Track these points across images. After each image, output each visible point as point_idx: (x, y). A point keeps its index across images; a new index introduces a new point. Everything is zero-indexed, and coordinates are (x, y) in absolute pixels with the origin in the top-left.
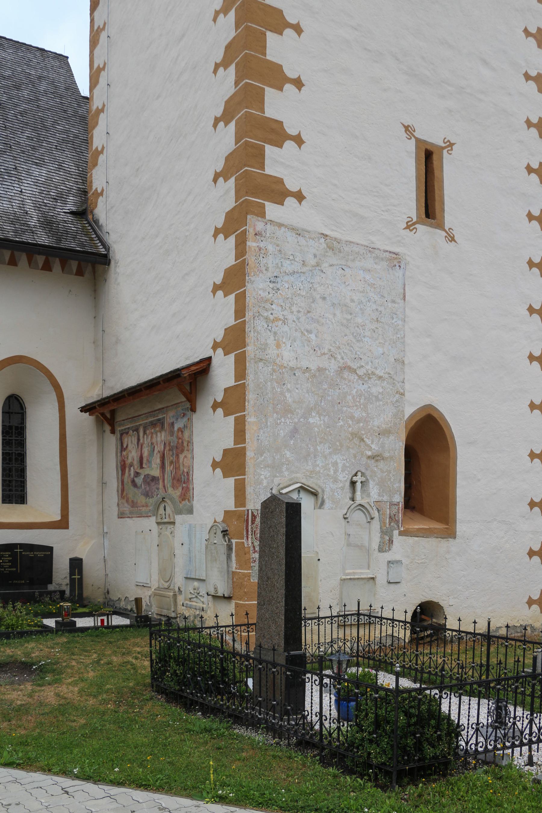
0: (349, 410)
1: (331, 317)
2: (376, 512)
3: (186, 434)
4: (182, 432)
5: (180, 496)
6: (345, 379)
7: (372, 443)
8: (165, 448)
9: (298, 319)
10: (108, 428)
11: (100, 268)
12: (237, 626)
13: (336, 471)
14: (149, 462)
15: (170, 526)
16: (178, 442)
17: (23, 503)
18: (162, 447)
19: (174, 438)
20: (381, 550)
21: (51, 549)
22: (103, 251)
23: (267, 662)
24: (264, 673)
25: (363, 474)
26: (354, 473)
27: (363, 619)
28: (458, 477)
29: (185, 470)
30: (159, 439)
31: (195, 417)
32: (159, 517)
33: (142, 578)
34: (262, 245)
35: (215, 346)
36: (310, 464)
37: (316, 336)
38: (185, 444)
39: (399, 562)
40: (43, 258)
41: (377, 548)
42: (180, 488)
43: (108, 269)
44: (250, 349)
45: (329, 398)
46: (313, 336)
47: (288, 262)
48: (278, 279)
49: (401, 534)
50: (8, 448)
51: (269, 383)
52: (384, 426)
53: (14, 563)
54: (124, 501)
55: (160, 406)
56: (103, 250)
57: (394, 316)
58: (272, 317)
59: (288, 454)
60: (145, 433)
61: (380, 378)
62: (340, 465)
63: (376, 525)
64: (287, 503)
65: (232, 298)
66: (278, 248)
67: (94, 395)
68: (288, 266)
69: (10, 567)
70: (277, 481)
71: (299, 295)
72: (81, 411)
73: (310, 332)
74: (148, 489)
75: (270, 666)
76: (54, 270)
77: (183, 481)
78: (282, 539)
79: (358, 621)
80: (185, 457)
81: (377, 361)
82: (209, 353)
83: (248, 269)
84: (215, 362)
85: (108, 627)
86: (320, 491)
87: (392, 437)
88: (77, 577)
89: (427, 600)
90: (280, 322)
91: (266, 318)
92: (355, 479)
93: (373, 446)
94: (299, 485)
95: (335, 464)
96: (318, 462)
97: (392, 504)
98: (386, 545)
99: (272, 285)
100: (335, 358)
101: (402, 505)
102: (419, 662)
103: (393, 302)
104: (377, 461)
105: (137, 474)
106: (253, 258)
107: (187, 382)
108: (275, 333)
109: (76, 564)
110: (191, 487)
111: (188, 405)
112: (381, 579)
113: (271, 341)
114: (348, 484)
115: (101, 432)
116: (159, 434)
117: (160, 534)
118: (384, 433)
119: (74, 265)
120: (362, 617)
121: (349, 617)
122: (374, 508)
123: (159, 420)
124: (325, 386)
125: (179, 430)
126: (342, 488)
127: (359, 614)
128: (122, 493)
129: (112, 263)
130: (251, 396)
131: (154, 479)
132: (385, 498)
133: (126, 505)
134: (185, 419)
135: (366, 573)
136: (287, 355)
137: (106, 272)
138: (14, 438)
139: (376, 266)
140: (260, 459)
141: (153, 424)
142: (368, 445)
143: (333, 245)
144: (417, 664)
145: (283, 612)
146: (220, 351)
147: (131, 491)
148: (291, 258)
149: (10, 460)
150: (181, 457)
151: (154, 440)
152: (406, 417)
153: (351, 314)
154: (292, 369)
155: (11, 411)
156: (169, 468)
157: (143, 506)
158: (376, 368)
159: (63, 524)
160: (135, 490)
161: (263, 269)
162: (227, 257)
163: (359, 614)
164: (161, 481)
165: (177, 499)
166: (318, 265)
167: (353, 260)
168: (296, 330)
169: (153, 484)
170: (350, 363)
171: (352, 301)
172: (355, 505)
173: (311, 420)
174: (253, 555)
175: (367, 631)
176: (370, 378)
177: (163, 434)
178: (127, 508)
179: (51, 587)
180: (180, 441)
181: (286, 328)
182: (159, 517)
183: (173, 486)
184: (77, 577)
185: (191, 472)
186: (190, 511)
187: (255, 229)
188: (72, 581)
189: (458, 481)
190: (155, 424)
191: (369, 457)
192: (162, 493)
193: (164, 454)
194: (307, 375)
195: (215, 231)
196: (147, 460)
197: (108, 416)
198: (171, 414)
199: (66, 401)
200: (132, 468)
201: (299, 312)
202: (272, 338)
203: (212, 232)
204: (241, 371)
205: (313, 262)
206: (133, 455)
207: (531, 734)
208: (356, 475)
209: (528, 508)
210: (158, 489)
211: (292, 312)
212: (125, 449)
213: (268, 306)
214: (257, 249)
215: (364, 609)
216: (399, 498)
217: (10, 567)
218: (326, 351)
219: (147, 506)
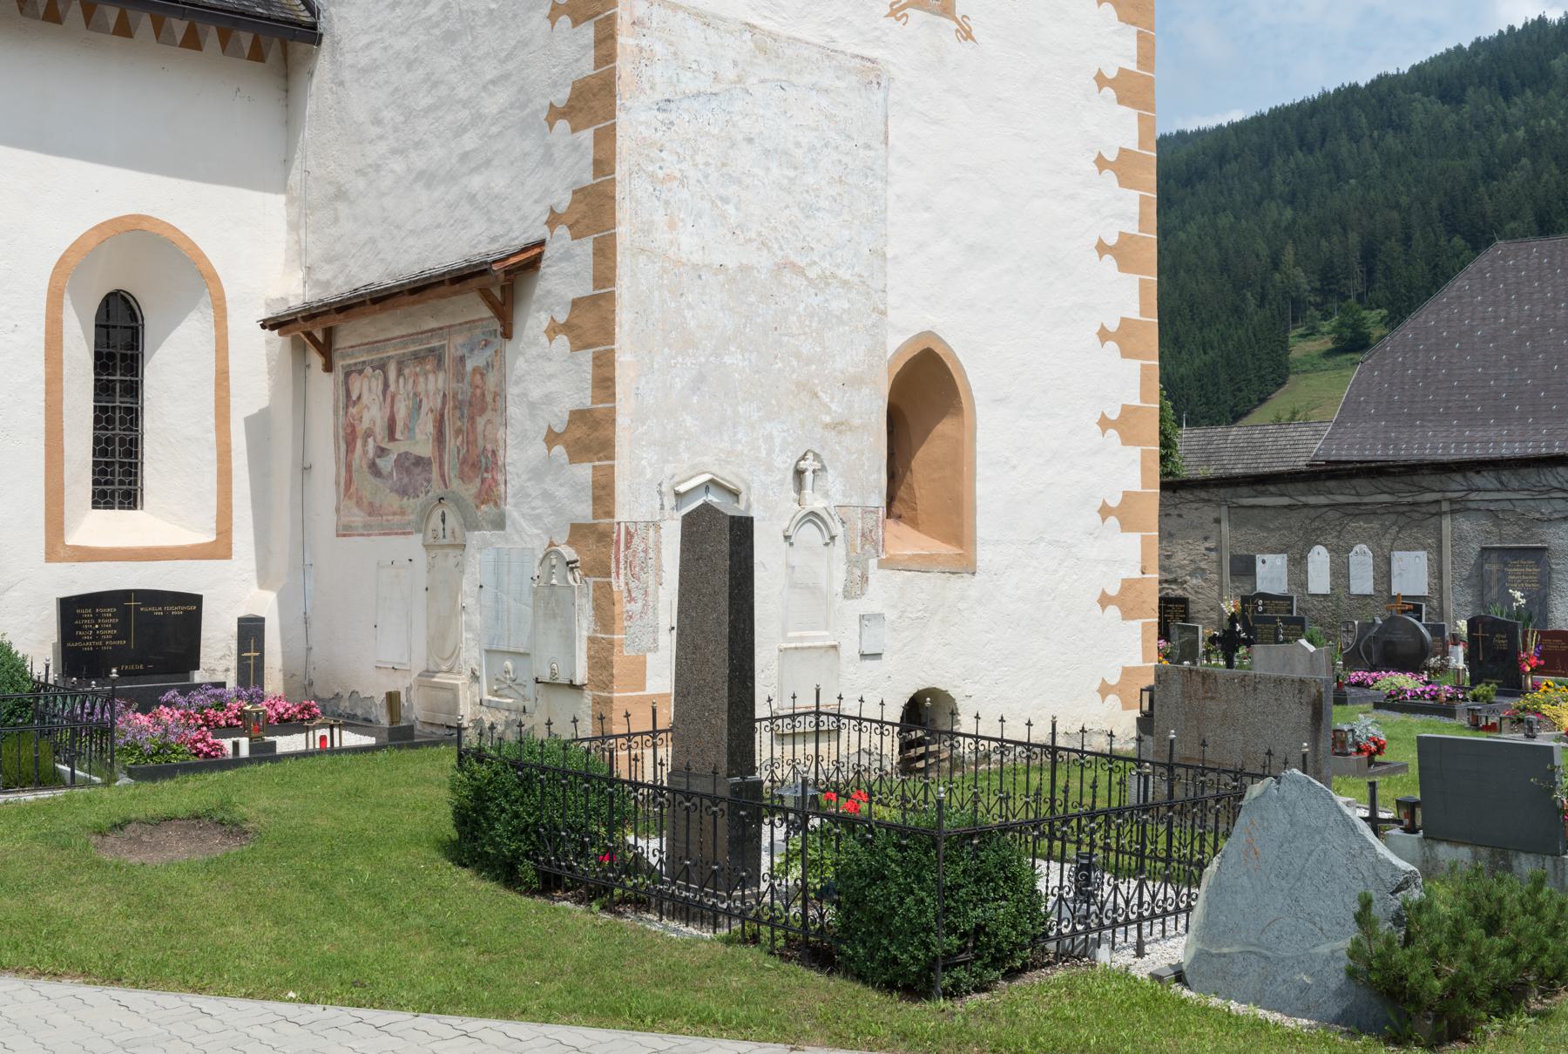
0: (792, 341)
1: (761, 173)
2: (839, 525)
3: (492, 379)
4: (482, 375)
5: (478, 495)
6: (786, 286)
7: (832, 400)
8: (444, 404)
9: (706, 177)
10: (316, 360)
11: (301, 47)
12: (778, 718)
13: (770, 452)
14: (409, 429)
15: (452, 553)
16: (473, 395)
17: (135, 507)
18: (439, 401)
19: (465, 386)
20: (847, 595)
21: (197, 600)
22: (305, 16)
23: (702, 796)
24: (694, 816)
25: (817, 456)
26: (801, 454)
27: (827, 723)
28: (979, 461)
29: (489, 447)
30: (431, 387)
31: (509, 346)
32: (430, 533)
33: (390, 652)
34: (644, 42)
35: (554, 219)
36: (726, 438)
37: (737, 209)
38: (489, 398)
39: (879, 617)
40: (185, 24)
41: (840, 590)
42: (478, 480)
43: (317, 52)
44: (624, 232)
45: (759, 320)
46: (730, 209)
47: (689, 74)
48: (672, 105)
49: (882, 565)
50: (104, 397)
51: (656, 293)
52: (851, 370)
53: (123, 631)
54: (352, 503)
55: (434, 324)
56: (307, 13)
57: (870, 173)
58: (660, 174)
59: (689, 421)
60: (400, 373)
61: (845, 283)
62: (778, 441)
63: (839, 548)
64: (733, 517)
65: (587, 135)
66: (672, 49)
67: (294, 292)
68: (689, 83)
69: (115, 638)
70: (669, 469)
71: (708, 133)
72: (263, 327)
73: (725, 200)
74: (406, 480)
75: (706, 802)
76: (205, 48)
77: (482, 466)
78: (722, 581)
79: (817, 725)
80: (489, 421)
81: (839, 253)
82: (539, 232)
83: (620, 87)
84: (549, 251)
85: (333, 751)
86: (742, 487)
87: (866, 391)
88: (253, 654)
89: (927, 686)
90: (676, 183)
91: (652, 176)
92: (803, 465)
93: (834, 407)
94: (707, 477)
95: (769, 438)
96: (740, 436)
97: (866, 511)
98: (857, 585)
99: (661, 116)
100: (769, 249)
101: (882, 512)
102: (930, 798)
103: (868, 147)
104: (840, 432)
105: (382, 452)
106: (630, 67)
107: (500, 284)
108: (667, 203)
109: (250, 631)
110: (500, 478)
111: (497, 325)
112: (850, 650)
113: (659, 218)
114: (790, 474)
115: (300, 365)
116: (431, 377)
117: (431, 568)
118: (853, 382)
119: (246, 39)
120: (823, 718)
121: (801, 718)
122: (836, 518)
123: (432, 350)
124: (752, 299)
125: (476, 370)
126: (782, 483)
127: (818, 714)
128: (347, 485)
129: (326, 40)
130: (624, 318)
131: (419, 461)
132: (855, 501)
133: (356, 510)
134: (489, 352)
135: (823, 637)
136: (688, 243)
137: (310, 57)
138: (118, 377)
139: (838, 83)
140: (641, 430)
141: (418, 358)
142: (825, 405)
143: (765, 45)
144: (926, 802)
145: (726, 707)
146: (562, 231)
147: (366, 484)
148: (694, 66)
149: (110, 421)
150: (480, 422)
151: (421, 388)
152: (889, 355)
153: (796, 168)
154: (695, 267)
155: (111, 323)
156: (452, 443)
157: (394, 514)
158: (838, 266)
159: (220, 549)
160: (378, 481)
161: (647, 86)
162: (577, 60)
163: (818, 714)
164: (435, 468)
165: (471, 501)
166: (740, 80)
167: (799, 72)
168: (702, 198)
169: (418, 470)
170: (793, 257)
171: (798, 145)
172: (804, 512)
173: (728, 360)
174: (629, 607)
175: (834, 744)
176: (828, 284)
177: (441, 375)
178: (358, 517)
179: (198, 677)
180: (478, 392)
181: (685, 194)
182: (430, 533)
183: (462, 477)
184: (253, 654)
185: (501, 452)
186: (499, 523)
187: (631, 14)
188: (241, 660)
189: (979, 470)
190: (424, 358)
191: (826, 426)
192: (436, 489)
193: (442, 416)
194: (721, 278)
195: (552, 9)
196: (405, 425)
197: (319, 336)
198: (459, 340)
199: (229, 305)
200: (370, 440)
201: (707, 164)
202: (662, 211)
203: (547, 11)
204: (604, 269)
205: (730, 74)
206: (372, 414)
207: (1140, 905)
208: (803, 458)
209: (1098, 517)
210: (429, 481)
211: (696, 165)
212: (355, 403)
213: (654, 153)
214: (636, 51)
215: (828, 702)
216: (878, 499)
217: (115, 638)
218: (754, 236)
219: (403, 513)
